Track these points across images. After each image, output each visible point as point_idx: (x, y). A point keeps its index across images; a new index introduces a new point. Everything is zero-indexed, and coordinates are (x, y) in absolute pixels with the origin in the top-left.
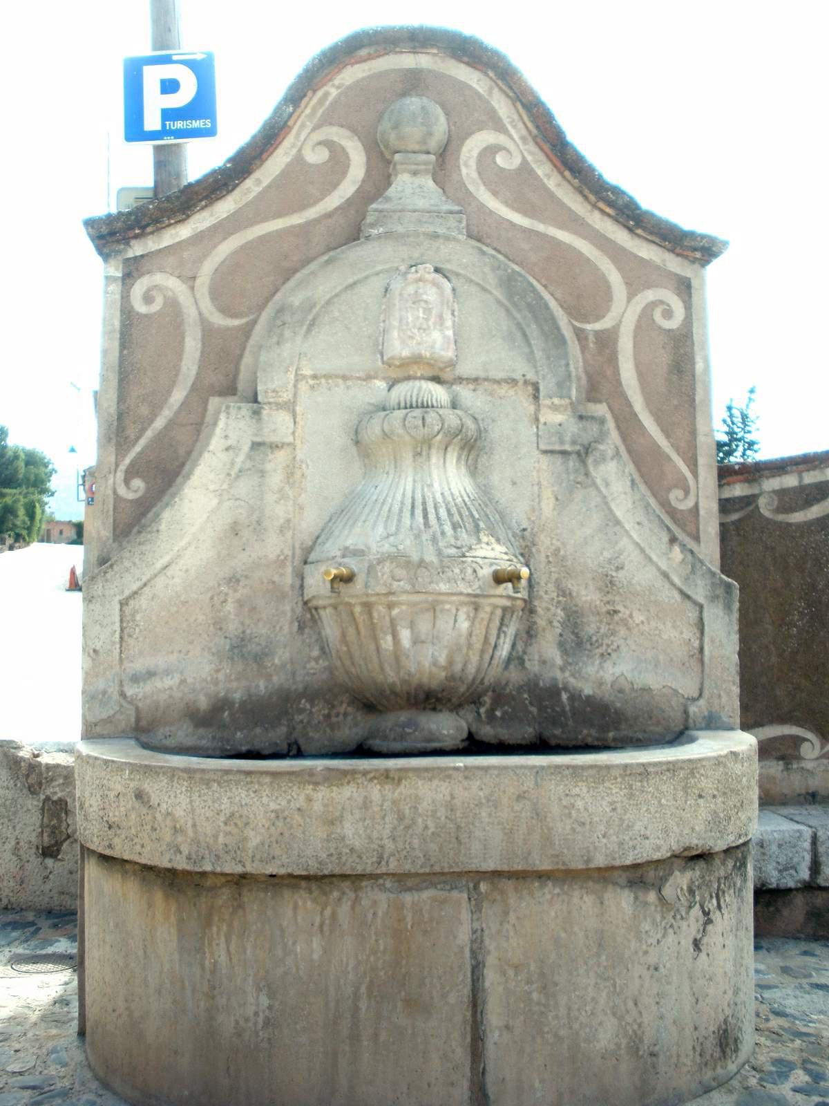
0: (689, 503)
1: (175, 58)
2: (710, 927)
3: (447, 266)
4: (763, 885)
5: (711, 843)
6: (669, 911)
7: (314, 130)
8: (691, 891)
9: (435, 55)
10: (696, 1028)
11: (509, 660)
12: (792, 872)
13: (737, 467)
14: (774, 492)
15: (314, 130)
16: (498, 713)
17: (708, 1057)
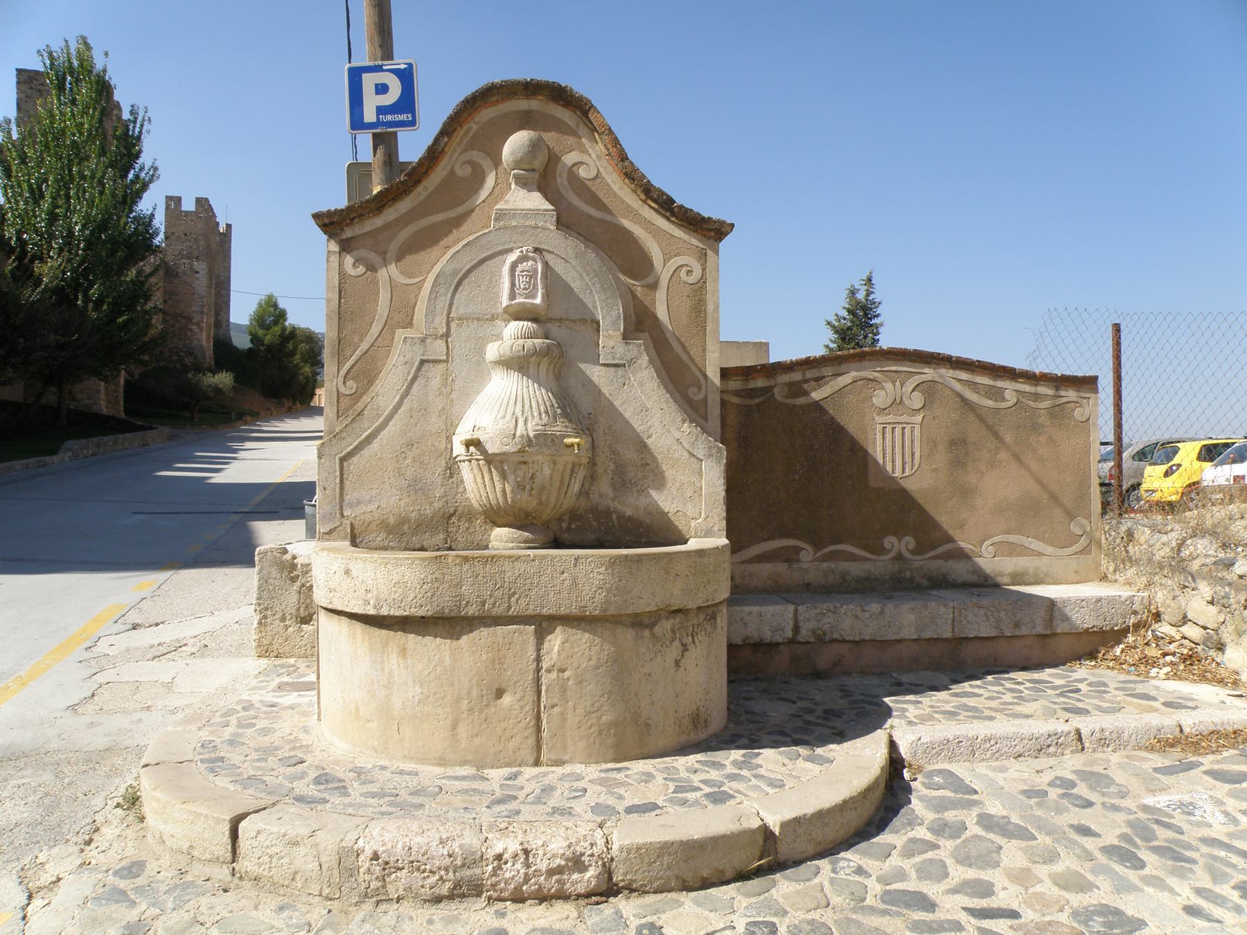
0: (701, 396)
1: (384, 68)
2: (686, 654)
3: (543, 247)
4: (761, 640)
5: (685, 603)
6: (658, 642)
7: (461, 154)
8: (673, 631)
9: (540, 100)
10: (676, 712)
11: (580, 493)
12: (781, 632)
13: (759, 367)
14: (785, 384)
15: (461, 154)
16: (573, 526)
17: (684, 728)
